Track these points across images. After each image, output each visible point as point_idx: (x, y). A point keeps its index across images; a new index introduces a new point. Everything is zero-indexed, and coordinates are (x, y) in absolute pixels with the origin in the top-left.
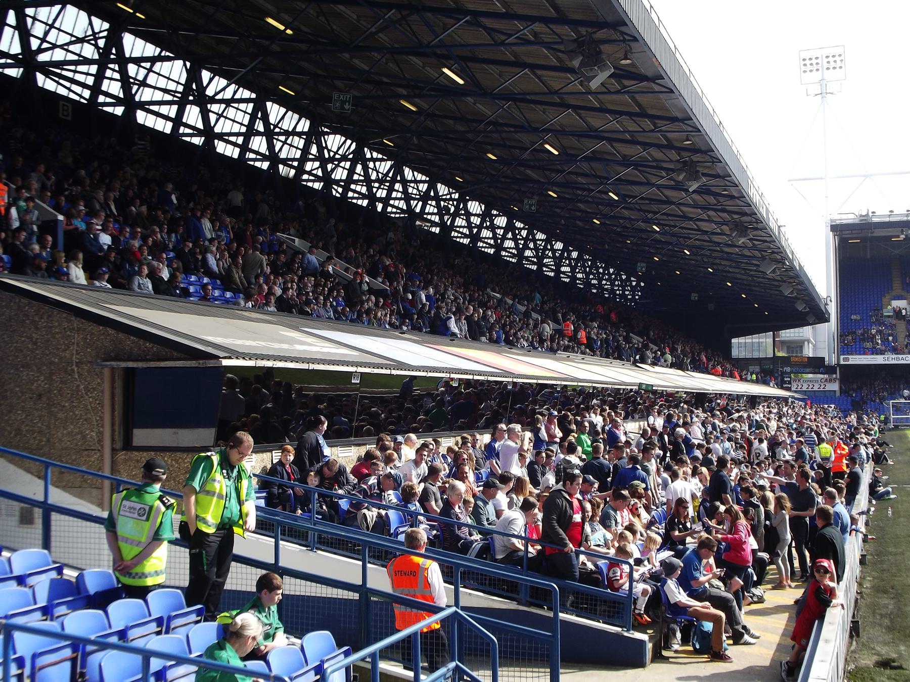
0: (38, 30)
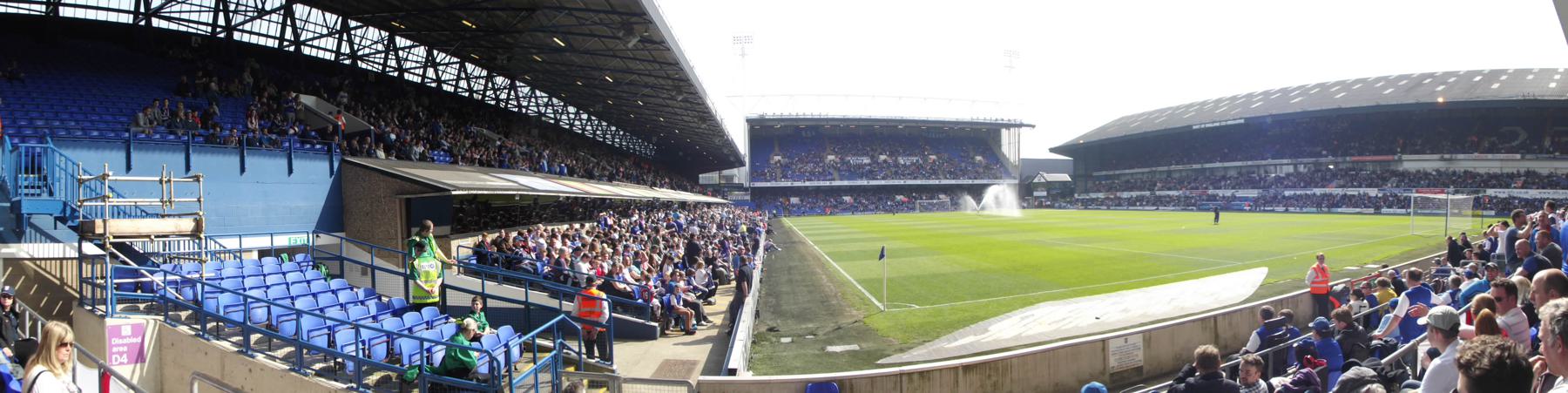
0: (357, 40)
